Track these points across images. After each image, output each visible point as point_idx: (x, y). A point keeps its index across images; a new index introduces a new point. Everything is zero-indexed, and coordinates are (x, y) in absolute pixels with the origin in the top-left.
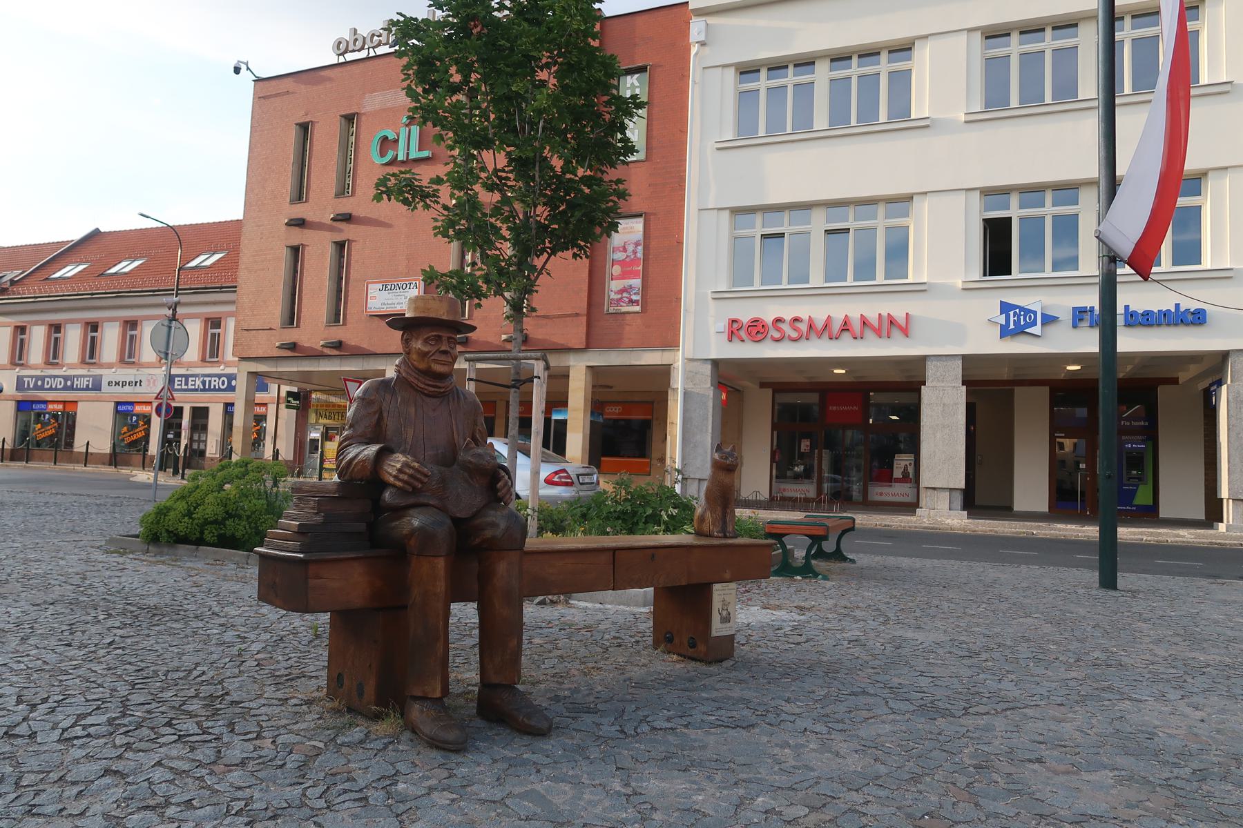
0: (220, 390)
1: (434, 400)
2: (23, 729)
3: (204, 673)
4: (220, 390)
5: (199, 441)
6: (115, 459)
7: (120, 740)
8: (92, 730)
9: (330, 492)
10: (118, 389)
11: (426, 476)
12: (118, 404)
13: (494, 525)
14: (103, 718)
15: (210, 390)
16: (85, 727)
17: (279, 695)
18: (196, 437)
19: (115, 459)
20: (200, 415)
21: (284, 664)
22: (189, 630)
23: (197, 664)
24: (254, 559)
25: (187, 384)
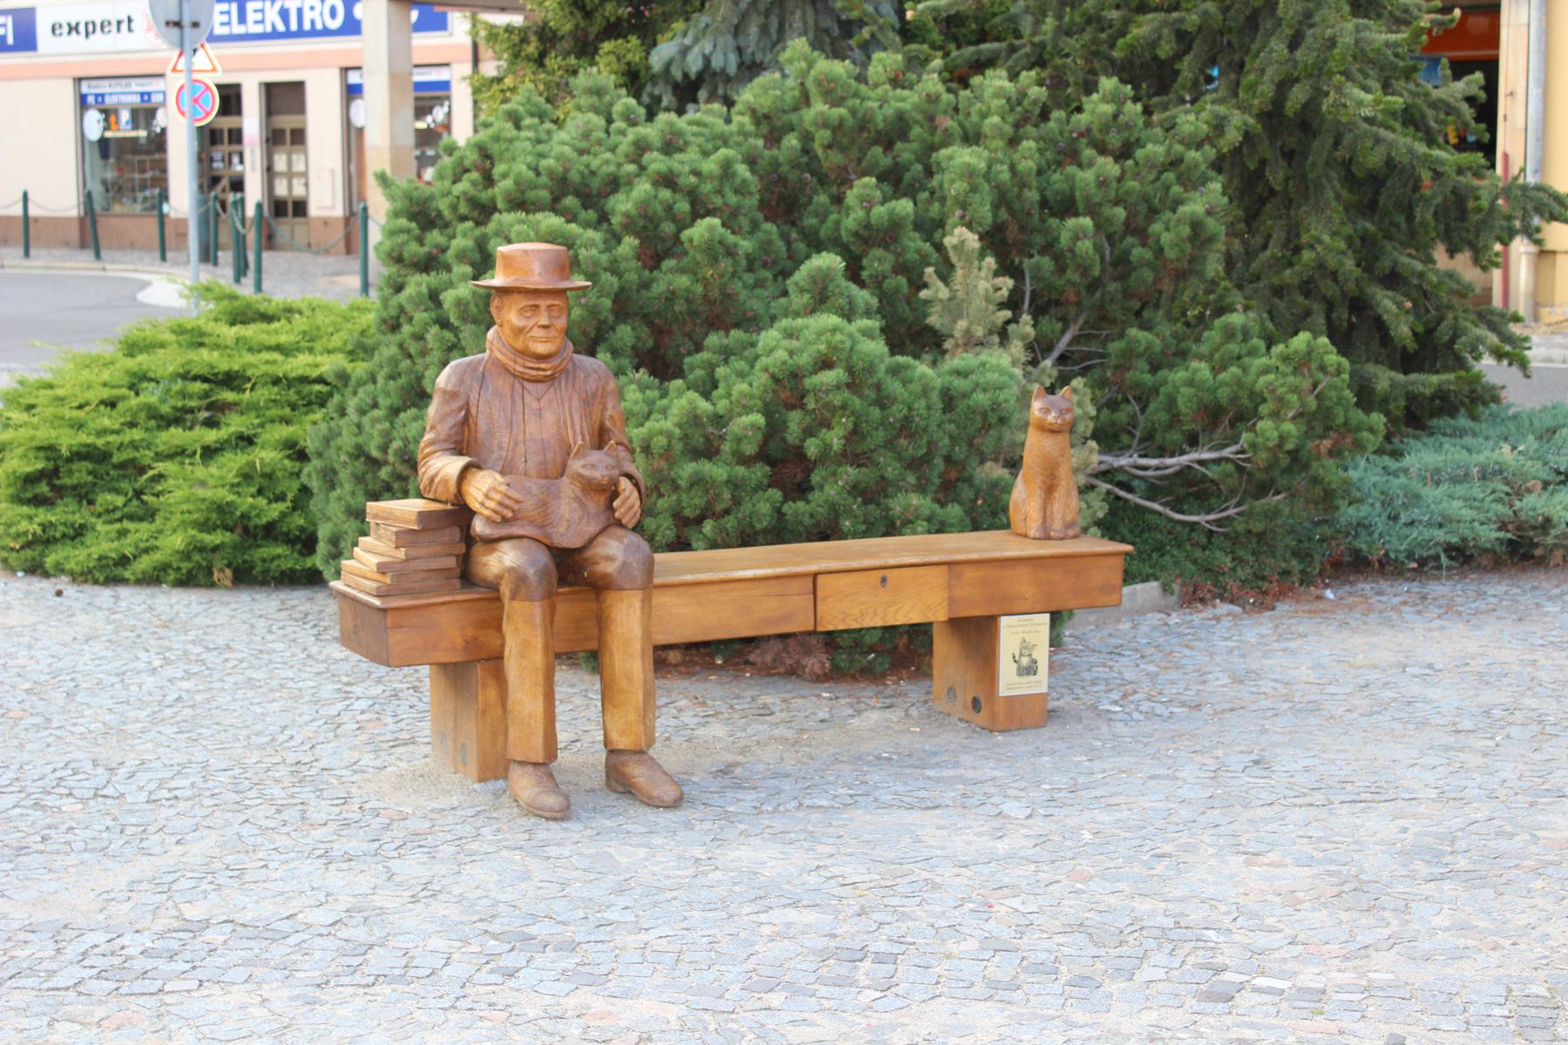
0: (326, 32)
1: (541, 386)
2: (109, 791)
3: (292, 738)
4: (326, 32)
5: (290, 175)
6: (89, 233)
7: (207, 802)
8: (177, 793)
9: (408, 522)
10: (77, 41)
11: (517, 502)
12: (79, 80)
13: (609, 559)
14: (186, 783)
15: (301, 33)
16: (170, 790)
17: (378, 763)
18: (280, 163)
19: (89, 233)
20: (284, 98)
21: (392, 727)
22: (274, 683)
23: (284, 728)
24: (333, 607)
25: (242, 19)
